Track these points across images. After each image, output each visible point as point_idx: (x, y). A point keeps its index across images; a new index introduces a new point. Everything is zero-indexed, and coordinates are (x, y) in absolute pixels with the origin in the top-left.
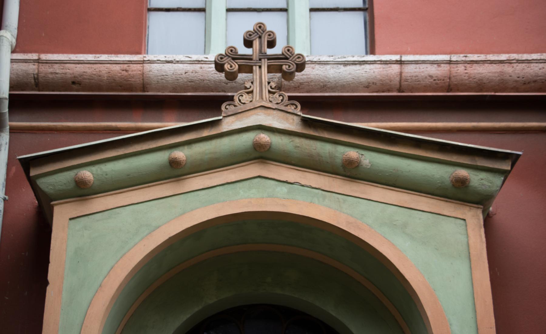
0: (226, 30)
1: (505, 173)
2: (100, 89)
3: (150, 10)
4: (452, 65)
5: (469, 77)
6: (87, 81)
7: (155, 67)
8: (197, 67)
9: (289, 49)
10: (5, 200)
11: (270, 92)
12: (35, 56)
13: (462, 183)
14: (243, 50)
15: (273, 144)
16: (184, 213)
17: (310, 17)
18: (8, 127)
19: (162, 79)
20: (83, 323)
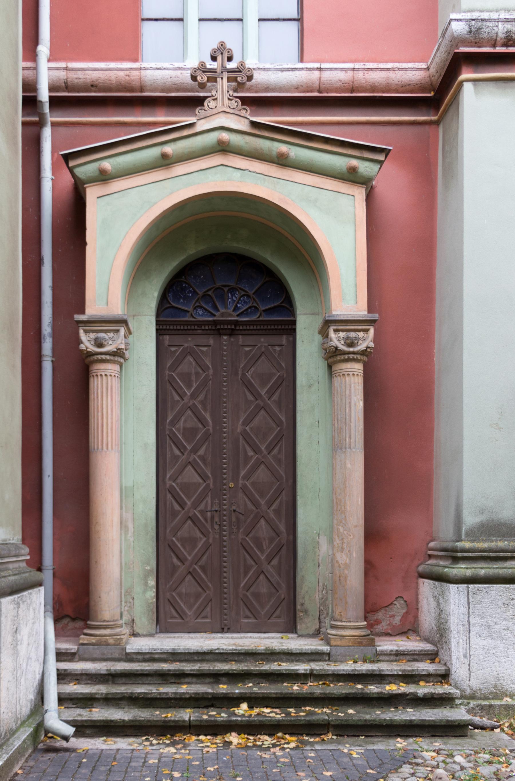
0: (199, 37)
1: (381, 163)
2: (110, 90)
3: (143, 20)
4: (355, 72)
5: (366, 81)
6: (101, 84)
7: (149, 73)
8: (178, 72)
9: (242, 64)
10: (52, 179)
11: (229, 99)
12: (63, 65)
13: (353, 170)
14: (210, 65)
15: (231, 140)
16: (172, 193)
17: (259, 26)
18: (49, 123)
19: (154, 83)
20: (111, 272)
